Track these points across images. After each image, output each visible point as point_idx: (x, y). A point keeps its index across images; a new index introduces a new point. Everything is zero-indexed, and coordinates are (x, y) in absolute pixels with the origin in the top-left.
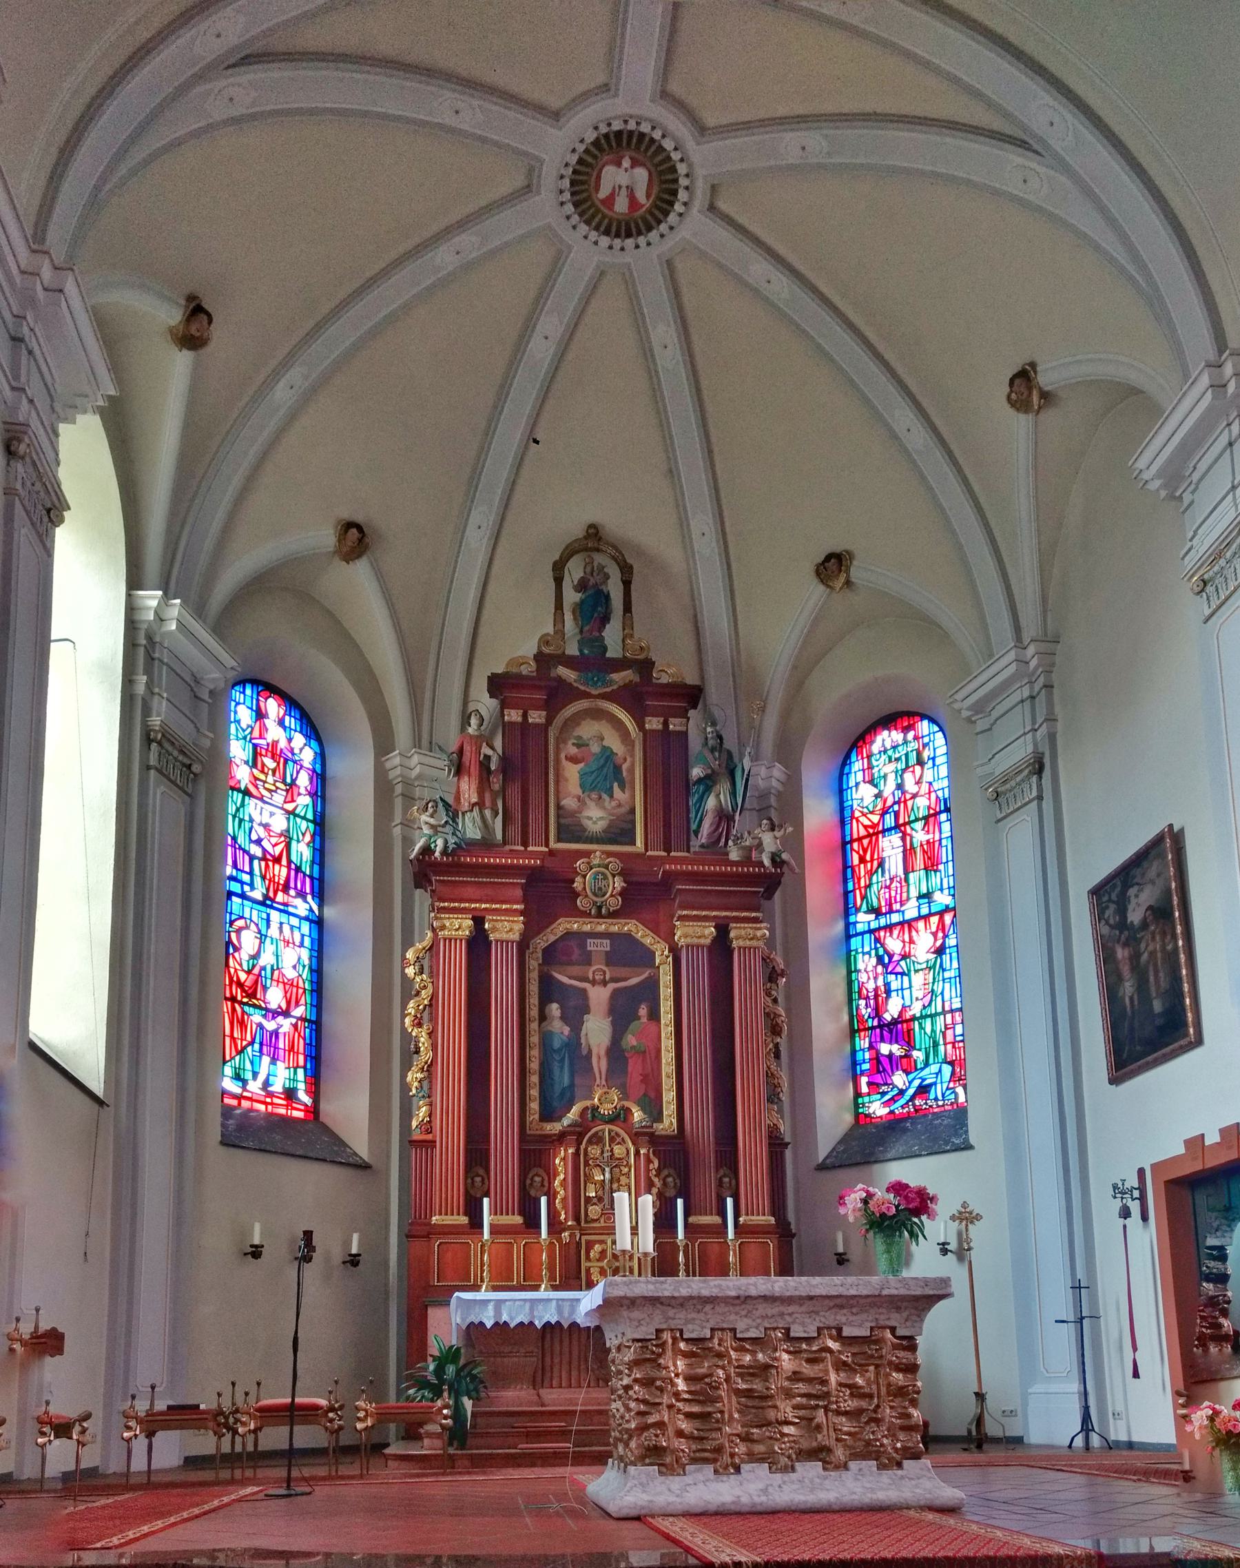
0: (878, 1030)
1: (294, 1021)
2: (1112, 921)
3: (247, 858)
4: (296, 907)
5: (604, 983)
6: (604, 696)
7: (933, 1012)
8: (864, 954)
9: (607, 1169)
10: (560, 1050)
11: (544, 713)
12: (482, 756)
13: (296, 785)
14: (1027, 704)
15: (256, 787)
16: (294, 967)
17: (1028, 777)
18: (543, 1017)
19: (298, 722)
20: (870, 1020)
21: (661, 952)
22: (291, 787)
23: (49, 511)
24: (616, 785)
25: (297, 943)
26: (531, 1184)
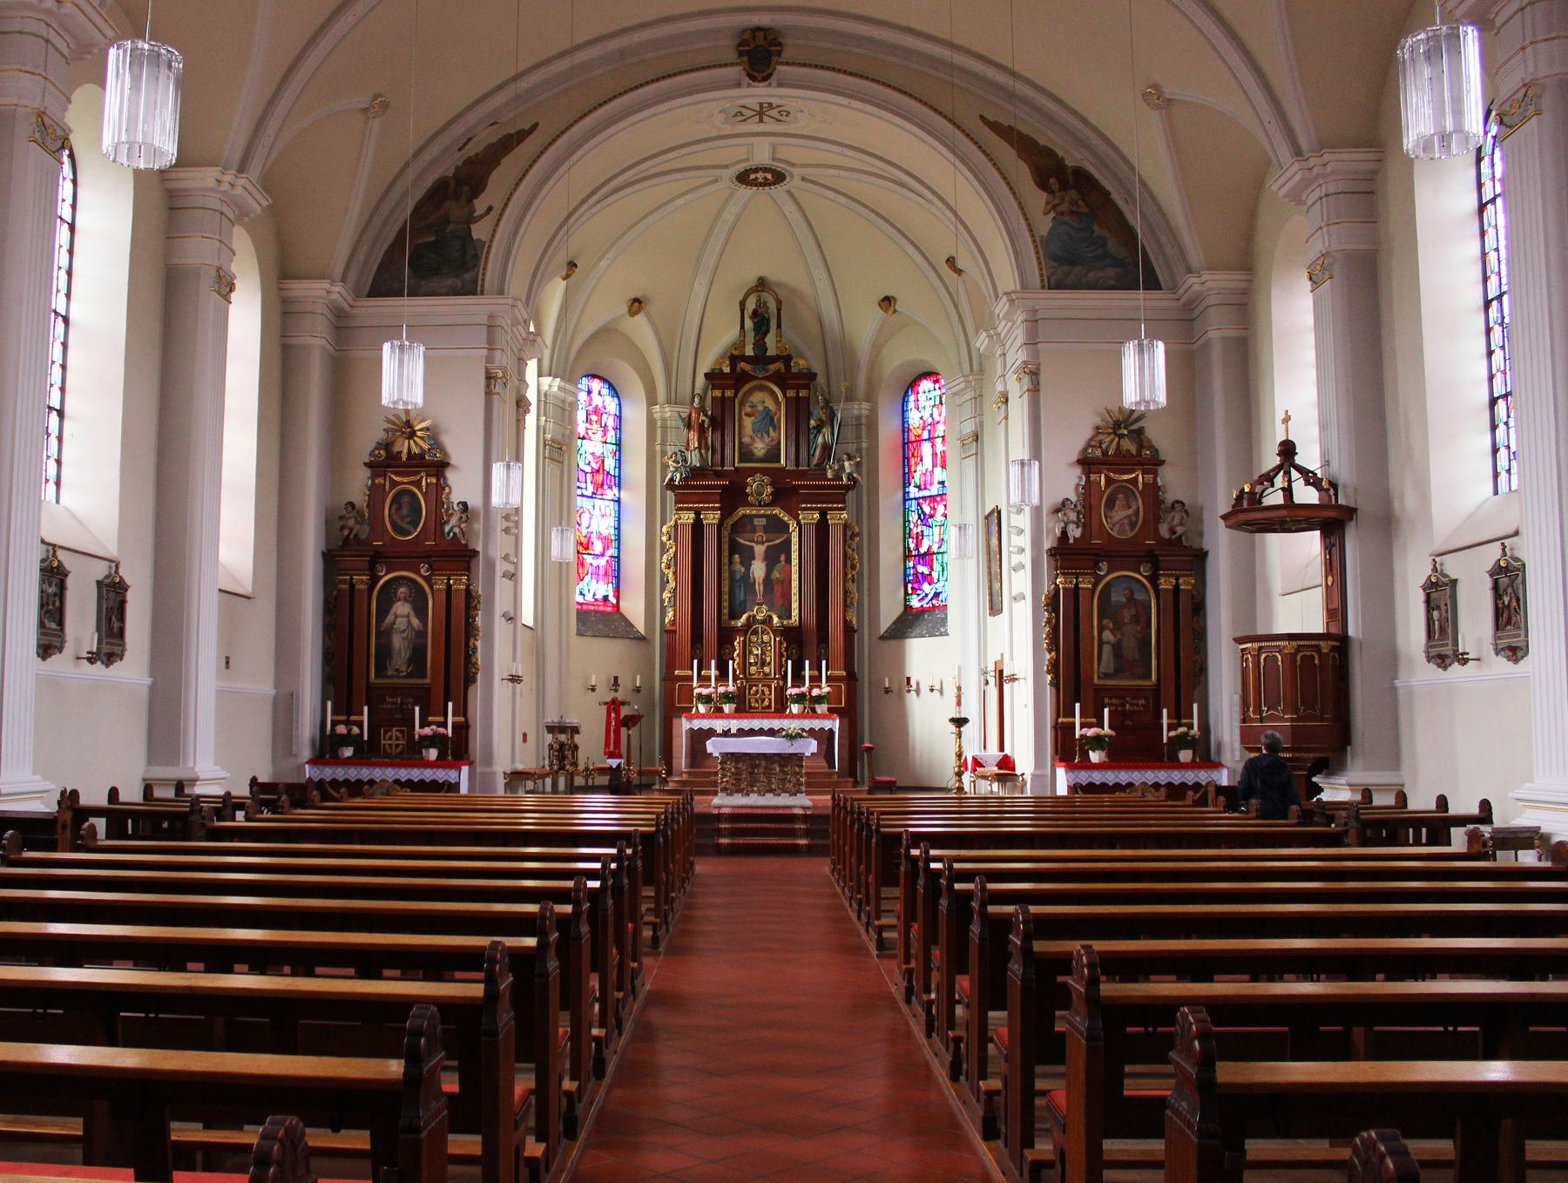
5: (763, 543)
6: (763, 379)
18: (731, 562)
21: (793, 525)
24: (771, 429)
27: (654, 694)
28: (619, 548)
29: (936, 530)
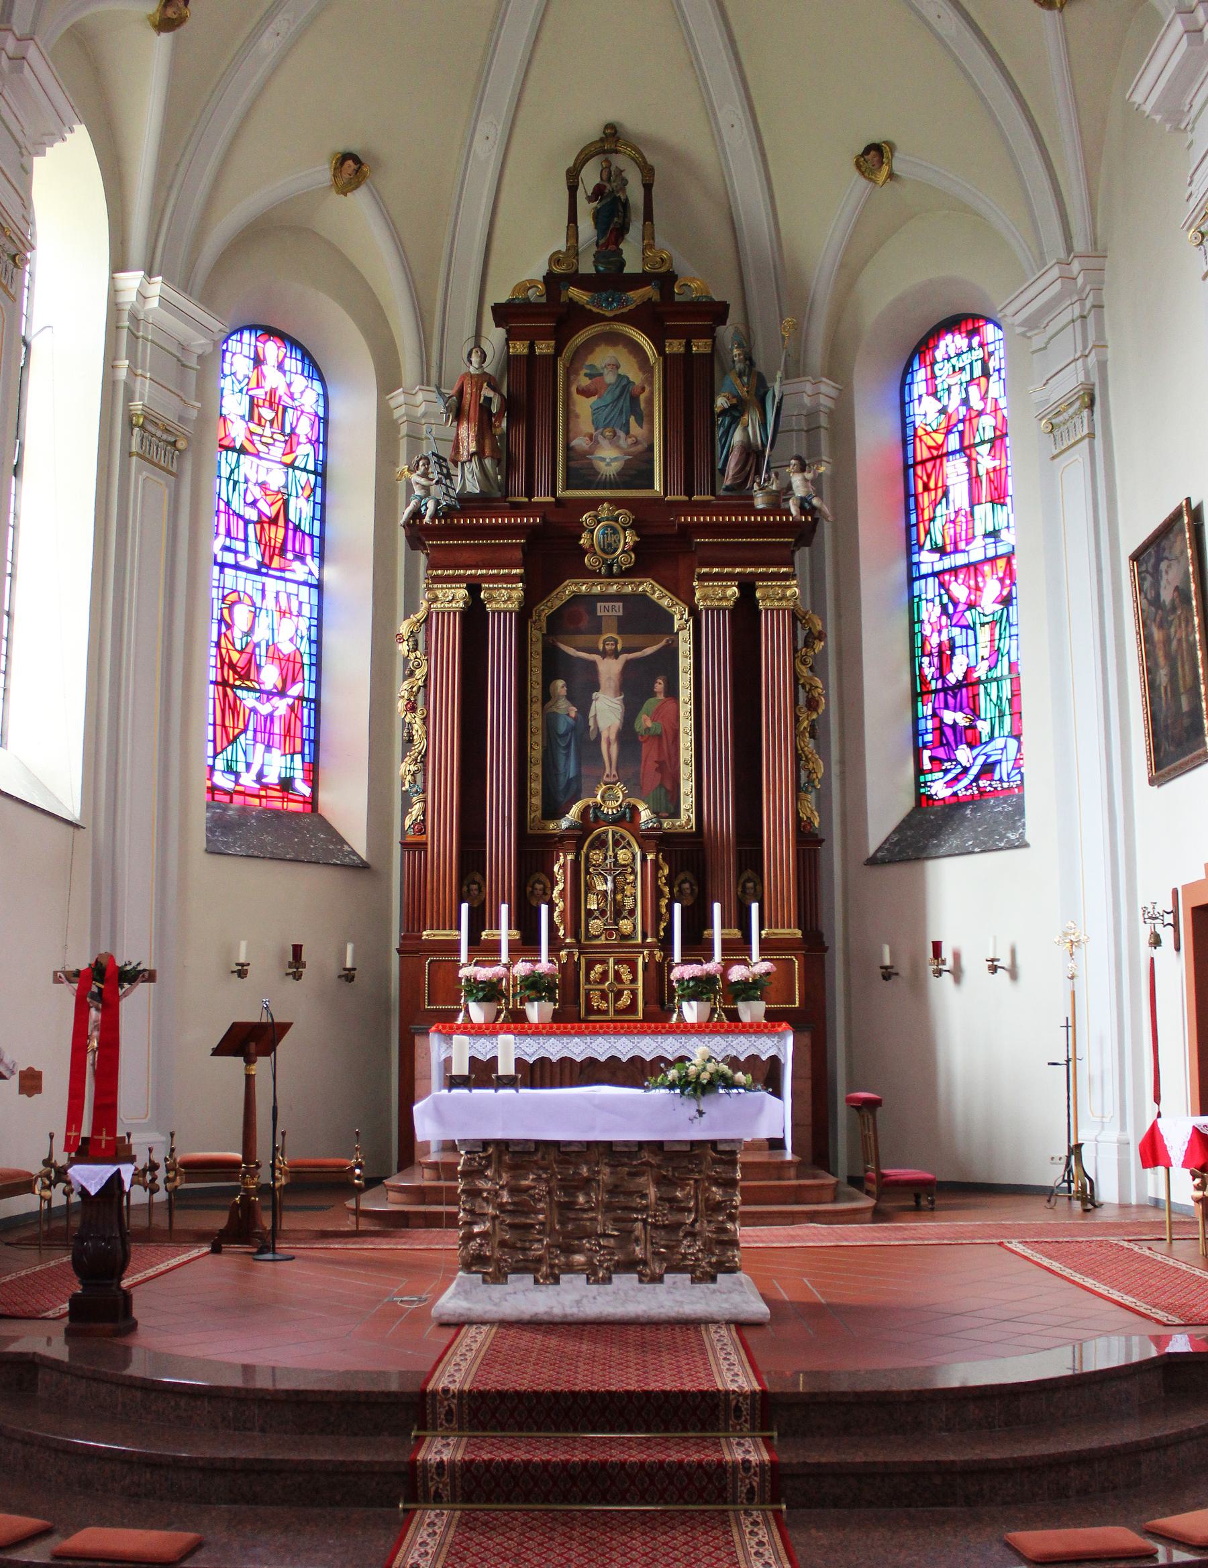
0: (942, 695)
1: (290, 701)
2: (1149, 596)
3: (241, 523)
4: (293, 571)
5: (616, 654)
6: (616, 319)
7: (999, 675)
8: (927, 601)
9: (609, 878)
10: (566, 734)
11: (552, 343)
12: (482, 398)
13: (295, 434)
14: (1078, 323)
15: (252, 442)
16: (291, 640)
17: (1080, 409)
18: (547, 696)
19: (299, 364)
20: (933, 682)
21: (680, 617)
22: (291, 438)
23: (13, 258)
24: (632, 419)
25: (295, 613)
26: (532, 892)
27: (388, 988)
28: (318, 683)
29: (984, 634)
